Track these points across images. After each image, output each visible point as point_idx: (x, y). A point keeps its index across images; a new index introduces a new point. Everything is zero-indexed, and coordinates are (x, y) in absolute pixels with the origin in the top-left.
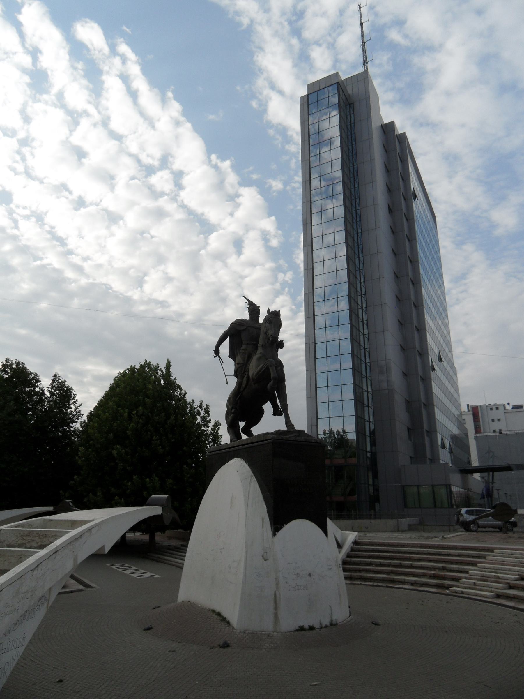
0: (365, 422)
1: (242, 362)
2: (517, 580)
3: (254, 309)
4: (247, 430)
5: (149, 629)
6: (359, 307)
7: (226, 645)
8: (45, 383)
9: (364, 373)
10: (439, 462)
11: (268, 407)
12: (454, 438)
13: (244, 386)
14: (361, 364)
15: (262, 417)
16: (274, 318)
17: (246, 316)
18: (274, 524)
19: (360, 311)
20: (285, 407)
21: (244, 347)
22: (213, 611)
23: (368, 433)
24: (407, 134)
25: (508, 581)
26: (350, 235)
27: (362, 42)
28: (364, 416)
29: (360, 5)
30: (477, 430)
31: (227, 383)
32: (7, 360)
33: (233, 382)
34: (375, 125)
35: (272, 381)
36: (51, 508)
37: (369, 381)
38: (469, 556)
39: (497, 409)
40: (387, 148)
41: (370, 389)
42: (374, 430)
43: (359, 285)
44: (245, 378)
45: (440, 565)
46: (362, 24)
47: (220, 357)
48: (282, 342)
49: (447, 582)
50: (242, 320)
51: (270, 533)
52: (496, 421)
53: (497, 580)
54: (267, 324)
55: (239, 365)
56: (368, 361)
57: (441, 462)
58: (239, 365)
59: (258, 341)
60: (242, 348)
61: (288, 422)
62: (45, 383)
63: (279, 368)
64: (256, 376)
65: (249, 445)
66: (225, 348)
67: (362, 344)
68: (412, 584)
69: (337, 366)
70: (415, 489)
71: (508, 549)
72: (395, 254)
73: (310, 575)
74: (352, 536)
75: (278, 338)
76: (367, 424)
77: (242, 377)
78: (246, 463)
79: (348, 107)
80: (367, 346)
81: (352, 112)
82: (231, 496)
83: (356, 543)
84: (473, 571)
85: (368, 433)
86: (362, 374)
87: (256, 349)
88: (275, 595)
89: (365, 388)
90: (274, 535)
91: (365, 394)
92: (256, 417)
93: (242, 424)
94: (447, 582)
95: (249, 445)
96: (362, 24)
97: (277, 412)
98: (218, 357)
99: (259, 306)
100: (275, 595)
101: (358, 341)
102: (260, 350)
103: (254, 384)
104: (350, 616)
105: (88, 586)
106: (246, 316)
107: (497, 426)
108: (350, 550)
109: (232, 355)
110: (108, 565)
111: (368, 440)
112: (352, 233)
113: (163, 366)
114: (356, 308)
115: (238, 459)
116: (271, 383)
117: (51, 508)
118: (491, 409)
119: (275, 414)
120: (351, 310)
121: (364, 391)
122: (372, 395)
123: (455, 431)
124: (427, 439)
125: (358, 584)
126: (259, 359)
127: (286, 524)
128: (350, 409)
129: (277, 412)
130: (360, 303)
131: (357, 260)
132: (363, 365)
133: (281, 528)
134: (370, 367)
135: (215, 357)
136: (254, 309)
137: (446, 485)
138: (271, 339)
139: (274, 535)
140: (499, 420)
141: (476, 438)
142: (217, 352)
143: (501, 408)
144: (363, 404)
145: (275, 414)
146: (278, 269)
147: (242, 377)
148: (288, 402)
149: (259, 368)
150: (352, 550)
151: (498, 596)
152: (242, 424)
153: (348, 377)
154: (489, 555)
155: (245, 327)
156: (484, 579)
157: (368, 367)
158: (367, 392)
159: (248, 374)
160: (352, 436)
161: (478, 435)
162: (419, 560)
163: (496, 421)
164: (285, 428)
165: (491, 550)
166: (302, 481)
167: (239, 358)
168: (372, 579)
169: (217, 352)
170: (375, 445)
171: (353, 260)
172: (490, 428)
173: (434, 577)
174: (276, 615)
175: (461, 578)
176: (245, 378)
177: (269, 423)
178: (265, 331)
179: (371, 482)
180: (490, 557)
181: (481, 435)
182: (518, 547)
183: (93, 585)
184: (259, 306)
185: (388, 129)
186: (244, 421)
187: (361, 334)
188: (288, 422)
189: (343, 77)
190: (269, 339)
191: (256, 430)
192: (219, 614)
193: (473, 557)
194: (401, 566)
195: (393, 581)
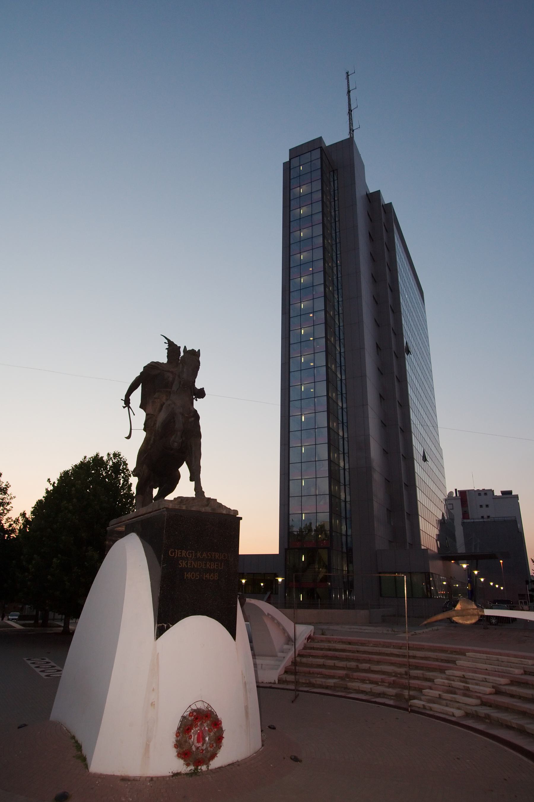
10: (421, 547)
22: (73, 737)
24: (393, 204)
25: (478, 695)
27: (349, 110)
29: (347, 73)
30: (465, 515)
31: (129, 437)
34: (360, 194)
38: (437, 660)
39: (486, 494)
40: (371, 217)
46: (349, 92)
48: (202, 390)
50: (158, 363)
52: (484, 506)
53: (467, 692)
57: (423, 547)
66: (136, 397)
71: (483, 652)
72: (378, 325)
74: (304, 631)
79: (332, 173)
81: (336, 178)
83: (309, 638)
90: (160, 632)
91: (342, 472)
96: (349, 92)
98: (127, 408)
107: (485, 512)
110: (25, 659)
118: (480, 494)
124: (407, 521)
125: (305, 691)
133: (168, 628)
135: (124, 407)
137: (425, 573)
139: (160, 632)
140: (487, 506)
141: (463, 524)
142: (127, 402)
150: (305, 648)
152: (155, 492)
154: (460, 660)
156: (452, 690)
161: (465, 521)
162: (378, 662)
163: (484, 506)
164: (193, 494)
165: (462, 653)
168: (380, 662)
169: (127, 402)
172: (476, 514)
181: (468, 521)
182: (494, 650)
185: (374, 198)
186: (155, 488)
189: (328, 142)
193: (442, 661)
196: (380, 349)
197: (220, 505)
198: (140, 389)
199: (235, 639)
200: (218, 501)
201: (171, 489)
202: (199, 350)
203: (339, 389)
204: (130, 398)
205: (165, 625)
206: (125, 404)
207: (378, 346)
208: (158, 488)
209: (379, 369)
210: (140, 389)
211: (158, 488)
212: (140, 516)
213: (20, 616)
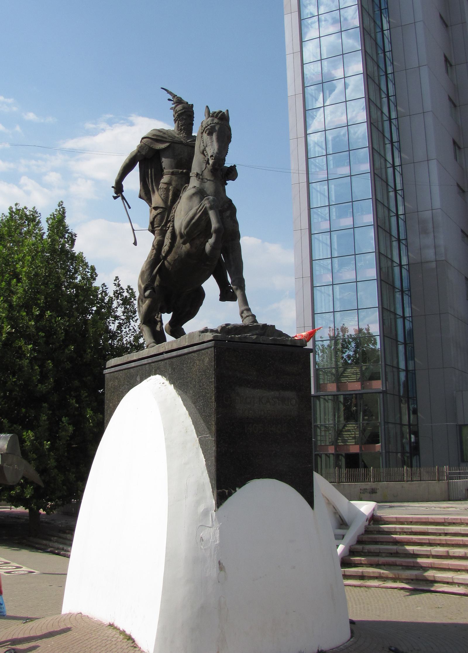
0: (395, 319)
1: (161, 204)
3: (185, 114)
4: (176, 330)
6: (385, 118)
9: (394, 233)
11: (211, 286)
13: (165, 248)
14: (390, 217)
15: (201, 304)
17: (168, 125)
18: (218, 489)
19: (387, 124)
20: (240, 283)
21: (165, 179)
23: (401, 338)
26: (374, 81)
28: (395, 309)
31: (135, 243)
33: (147, 241)
35: (214, 236)
37: (403, 247)
41: (404, 261)
42: (411, 331)
43: (383, 79)
44: (168, 235)
47: (123, 198)
54: (205, 135)
55: (158, 211)
56: (401, 211)
58: (158, 211)
59: (189, 169)
60: (163, 181)
63: (228, 213)
64: (186, 228)
65: (174, 354)
66: (133, 182)
67: (394, 233)
69: (347, 222)
75: (224, 160)
76: (400, 322)
77: (163, 233)
78: (171, 383)
80: (399, 187)
82: (147, 447)
85: (401, 338)
86: (391, 235)
87: (188, 182)
89: (396, 259)
91: (397, 270)
92: (188, 304)
93: (166, 318)
95: (174, 354)
97: (226, 295)
98: (120, 198)
99: (192, 106)
101: (384, 177)
102: (194, 182)
103: (184, 243)
104: (352, 637)
106: (168, 125)
108: (362, 530)
109: (146, 194)
111: (401, 348)
112: (373, 31)
114: (380, 120)
115: (158, 377)
116: (211, 241)
121: (395, 264)
122: (409, 271)
126: (191, 197)
127: (240, 487)
129: (226, 295)
130: (385, 110)
131: (379, 36)
132: (394, 220)
133: (230, 494)
134: (403, 198)
135: (115, 198)
136: (185, 114)
138: (211, 162)
142: (119, 189)
144: (394, 287)
146: (306, 337)
147: (163, 233)
148: (246, 274)
149: (191, 214)
153: (368, 239)
155: (168, 144)
157: (401, 222)
158: (401, 266)
159: (173, 226)
167: (157, 199)
169: (119, 189)
170: (413, 358)
171: (373, 35)
176: (168, 235)
177: (214, 313)
178: (202, 148)
184: (192, 106)
187: (392, 214)
190: (208, 162)
191: (190, 327)
194: (448, 557)
196: (451, 65)
197: (280, 333)
198: (137, 167)
199: (311, 503)
200: (277, 328)
201: (191, 314)
202: (227, 111)
203: (387, 135)
204: (123, 183)
205: (227, 491)
206: (116, 193)
207: (446, 60)
208: (172, 313)
209: (450, 99)
210: (137, 167)
211: (172, 313)
212: (162, 354)
213: (355, 442)
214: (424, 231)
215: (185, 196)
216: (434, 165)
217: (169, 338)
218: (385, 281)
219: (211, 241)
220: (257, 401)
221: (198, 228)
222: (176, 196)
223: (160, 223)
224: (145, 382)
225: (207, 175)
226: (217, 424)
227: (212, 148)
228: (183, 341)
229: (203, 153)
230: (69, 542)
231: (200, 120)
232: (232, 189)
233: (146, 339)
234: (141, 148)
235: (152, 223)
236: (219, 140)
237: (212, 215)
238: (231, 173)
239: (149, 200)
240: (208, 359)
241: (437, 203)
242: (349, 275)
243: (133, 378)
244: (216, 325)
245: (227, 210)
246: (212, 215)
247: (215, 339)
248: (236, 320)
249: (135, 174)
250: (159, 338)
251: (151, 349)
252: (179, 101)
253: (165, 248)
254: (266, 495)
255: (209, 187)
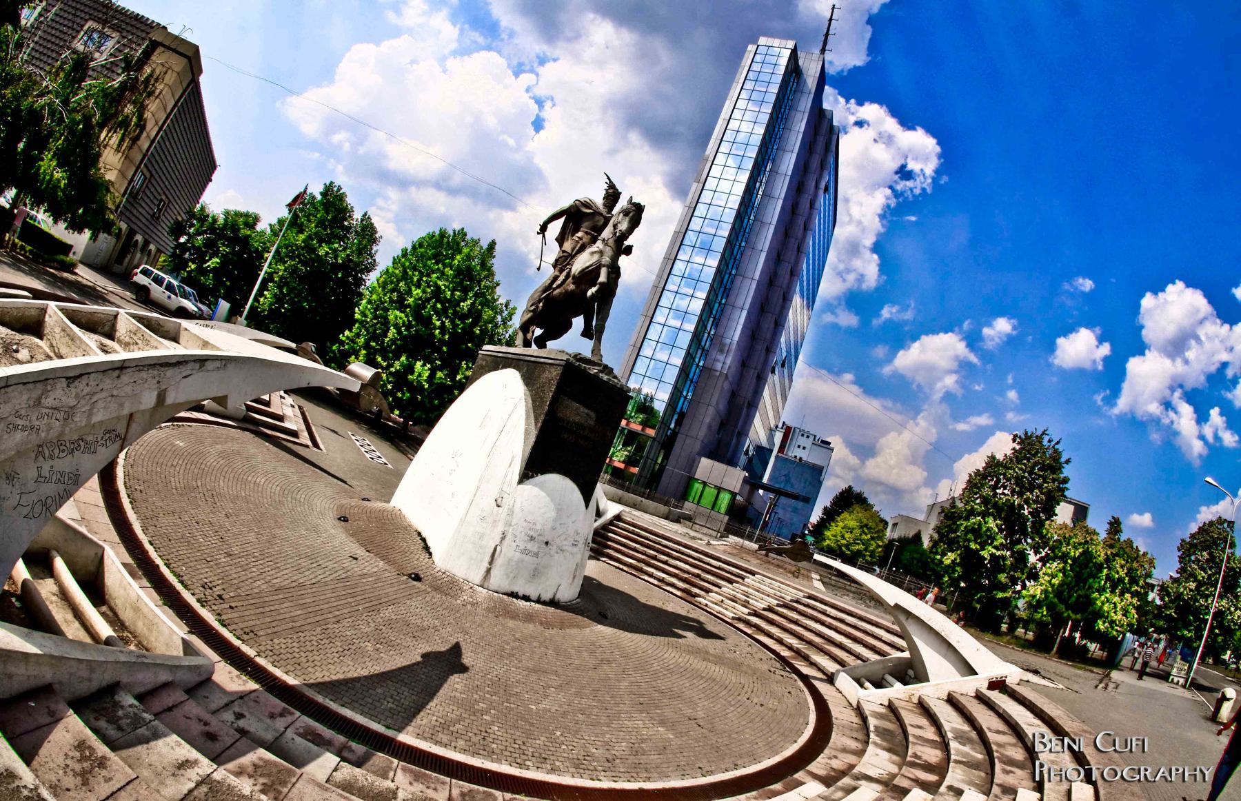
2: (764, 609)
3: (612, 195)
5: (346, 520)
7: (417, 578)
8: (357, 215)
11: (578, 322)
12: (759, 449)
13: (558, 282)
16: (636, 213)
17: (598, 199)
20: (601, 329)
21: (580, 234)
30: (781, 449)
32: (331, 183)
36: (293, 345)
44: (564, 273)
45: (696, 571)
49: (696, 590)
51: (517, 478)
53: (745, 604)
61: (596, 350)
62: (357, 215)
66: (556, 227)
68: (659, 580)
69: (677, 324)
70: (701, 486)
73: (547, 543)
77: (561, 271)
82: (493, 413)
84: (727, 589)
88: (495, 550)
92: (557, 328)
93: (538, 332)
94: (696, 590)
97: (587, 333)
100: (495, 550)
102: (599, 244)
105: (316, 445)
106: (598, 199)
109: (561, 240)
111: (676, 417)
113: (485, 244)
116: (594, 289)
117: (293, 345)
119: (584, 334)
120: (719, 271)
123: (764, 443)
128: (671, 375)
129: (587, 333)
136: (612, 195)
141: (777, 457)
142: (543, 228)
143: (812, 437)
145: (584, 334)
151: (739, 619)
153: (685, 340)
160: (660, 406)
165: (753, 573)
166: (577, 431)
169: (543, 228)
173: (681, 579)
174: (488, 571)
175: (711, 591)
176: (564, 273)
177: (573, 342)
179: (659, 461)
180: (750, 580)
183: (322, 446)
188: (596, 350)
192: (424, 540)
194: (655, 558)
195: (641, 570)
198: (563, 219)
199: (587, 506)
210: (563, 219)
214: (721, 351)
215: (588, 251)
216: (744, 313)
217: (534, 346)
218: (684, 370)
219: (594, 289)
220: (577, 413)
221: (589, 275)
222: (582, 249)
223: (563, 262)
224: (505, 371)
225: (611, 242)
226: (544, 422)
227: (624, 226)
228: (542, 353)
229: (615, 226)
230: (416, 450)
231: (622, 203)
232: (623, 261)
233: (519, 340)
234: (571, 207)
235: (557, 261)
236: (630, 221)
237: (604, 272)
238: (628, 251)
239: (561, 245)
240: (555, 373)
241: (736, 337)
242: (664, 357)
243: (499, 363)
244: (572, 350)
245: (615, 272)
246: (604, 272)
247: (567, 361)
248: (587, 354)
249: (560, 223)
250: (527, 344)
251: (519, 349)
252: (611, 186)
253: (558, 282)
254: (559, 485)
255: (609, 252)
